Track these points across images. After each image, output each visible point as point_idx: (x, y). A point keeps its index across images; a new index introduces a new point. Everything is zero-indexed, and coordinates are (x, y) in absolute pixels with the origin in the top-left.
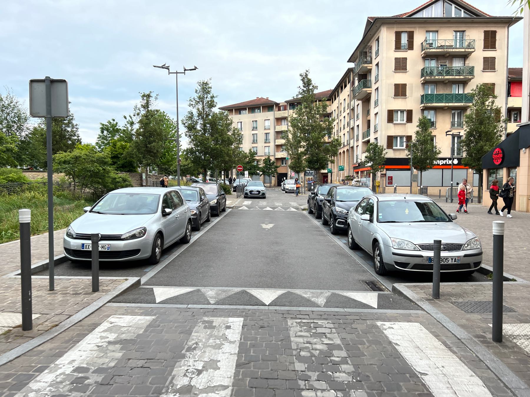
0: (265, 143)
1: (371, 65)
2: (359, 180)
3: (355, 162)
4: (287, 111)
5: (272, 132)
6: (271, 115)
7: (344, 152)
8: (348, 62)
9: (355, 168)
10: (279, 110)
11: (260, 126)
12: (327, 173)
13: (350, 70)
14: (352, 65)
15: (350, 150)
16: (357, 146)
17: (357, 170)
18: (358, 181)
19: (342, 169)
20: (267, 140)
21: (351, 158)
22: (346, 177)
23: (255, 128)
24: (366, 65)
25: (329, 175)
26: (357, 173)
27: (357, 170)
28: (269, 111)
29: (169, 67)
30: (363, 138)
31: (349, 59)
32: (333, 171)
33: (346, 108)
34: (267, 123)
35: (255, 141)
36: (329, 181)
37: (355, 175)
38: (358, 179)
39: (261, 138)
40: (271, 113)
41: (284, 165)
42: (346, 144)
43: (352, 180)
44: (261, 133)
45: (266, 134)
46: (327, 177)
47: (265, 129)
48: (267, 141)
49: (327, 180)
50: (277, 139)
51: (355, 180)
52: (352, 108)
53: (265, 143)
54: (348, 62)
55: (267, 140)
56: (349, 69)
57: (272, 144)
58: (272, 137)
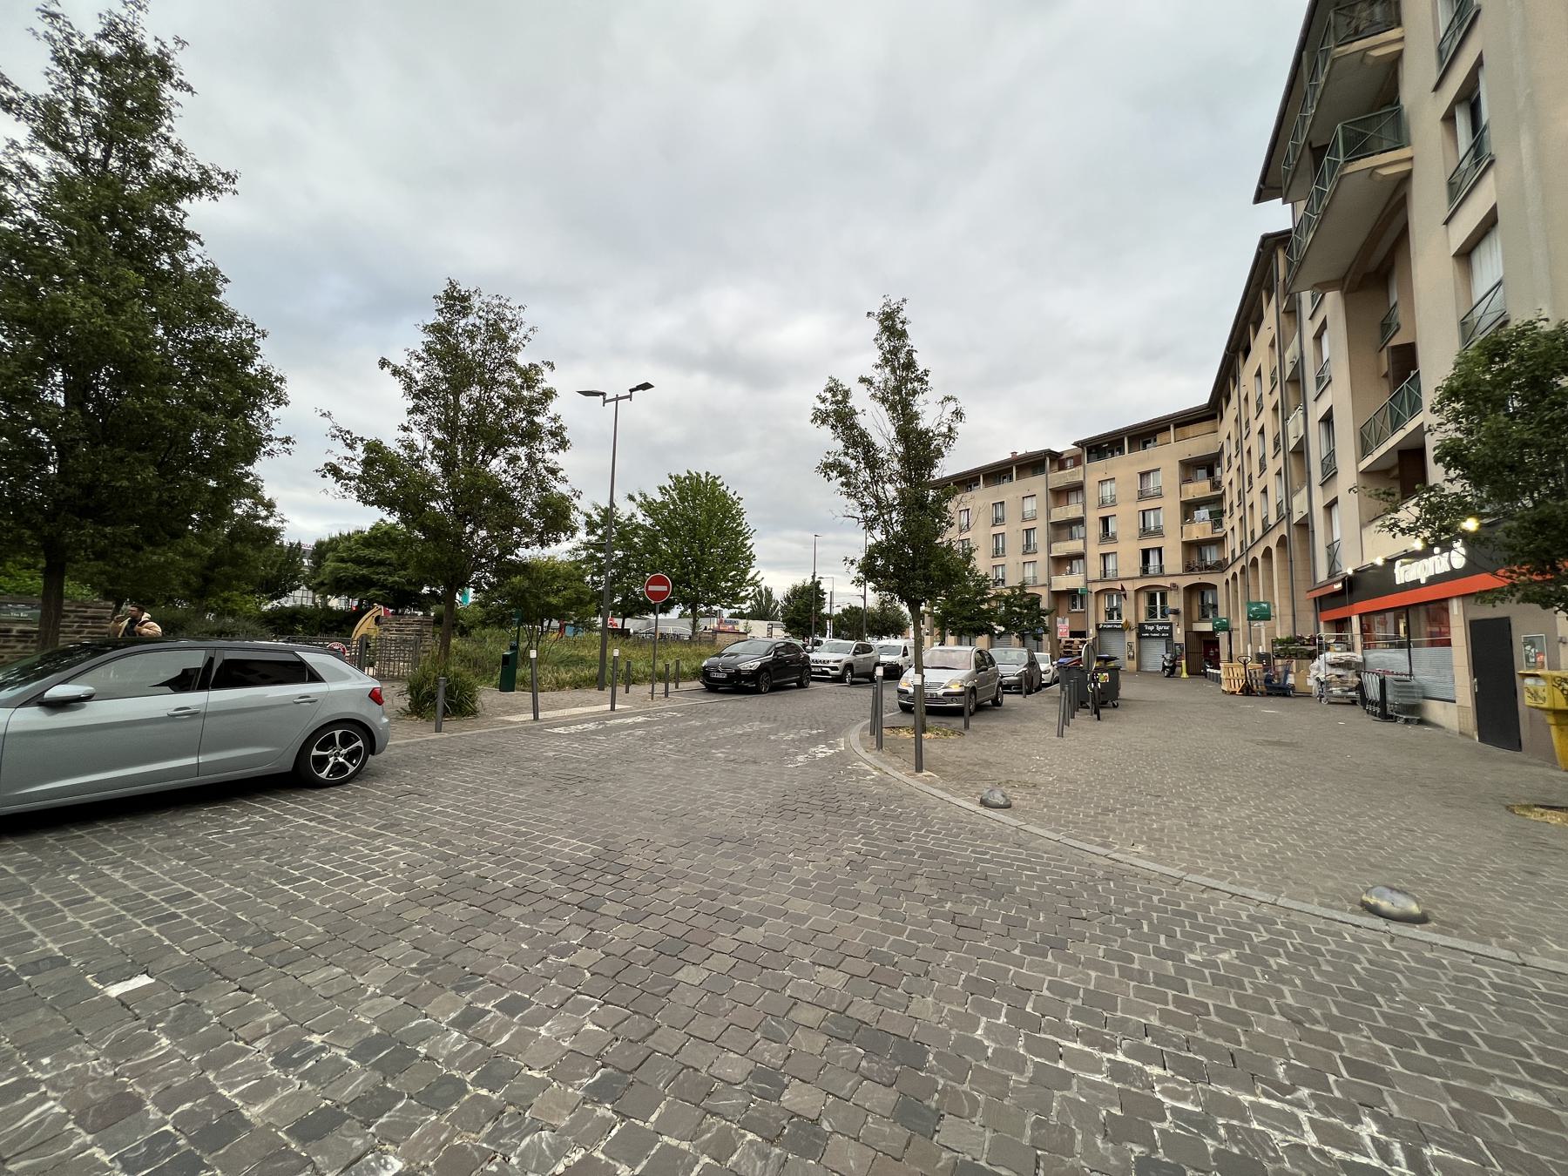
0: (1025, 553)
1: (1393, 34)
2: (1357, 656)
3: (1322, 575)
4: (1080, 468)
5: (1041, 526)
6: (1037, 484)
7: (1267, 553)
8: (1259, 198)
9: (1324, 602)
10: (1062, 467)
11: (1011, 513)
12: (1213, 633)
13: (1271, 245)
14: (1279, 216)
15: (1295, 545)
16: (1330, 507)
17: (1337, 614)
18: (1346, 665)
19: (1265, 616)
20: (1028, 546)
21: (1298, 565)
22: (1282, 642)
23: (998, 521)
24: (1358, 45)
25: (1223, 637)
26: (1341, 624)
27: (1337, 614)
28: (1035, 473)
29: (821, 417)
30: (1365, 450)
31: (1263, 179)
32: (1233, 625)
33: (1270, 452)
34: (1030, 505)
35: (997, 553)
36: (1224, 656)
37: (1325, 633)
38: (1346, 656)
39: (1014, 542)
40: (1040, 478)
41: (1078, 609)
42: (1272, 520)
43: (1312, 656)
44: (1012, 530)
45: (1028, 531)
46: (1216, 643)
47: (1024, 520)
48: (1028, 548)
49: (1217, 655)
50: (1058, 541)
51: (1329, 656)
52: (1292, 443)
53: (1025, 553)
54: (1259, 198)
55: (1028, 546)
56: (1266, 239)
57: (1042, 557)
58: (1040, 537)
